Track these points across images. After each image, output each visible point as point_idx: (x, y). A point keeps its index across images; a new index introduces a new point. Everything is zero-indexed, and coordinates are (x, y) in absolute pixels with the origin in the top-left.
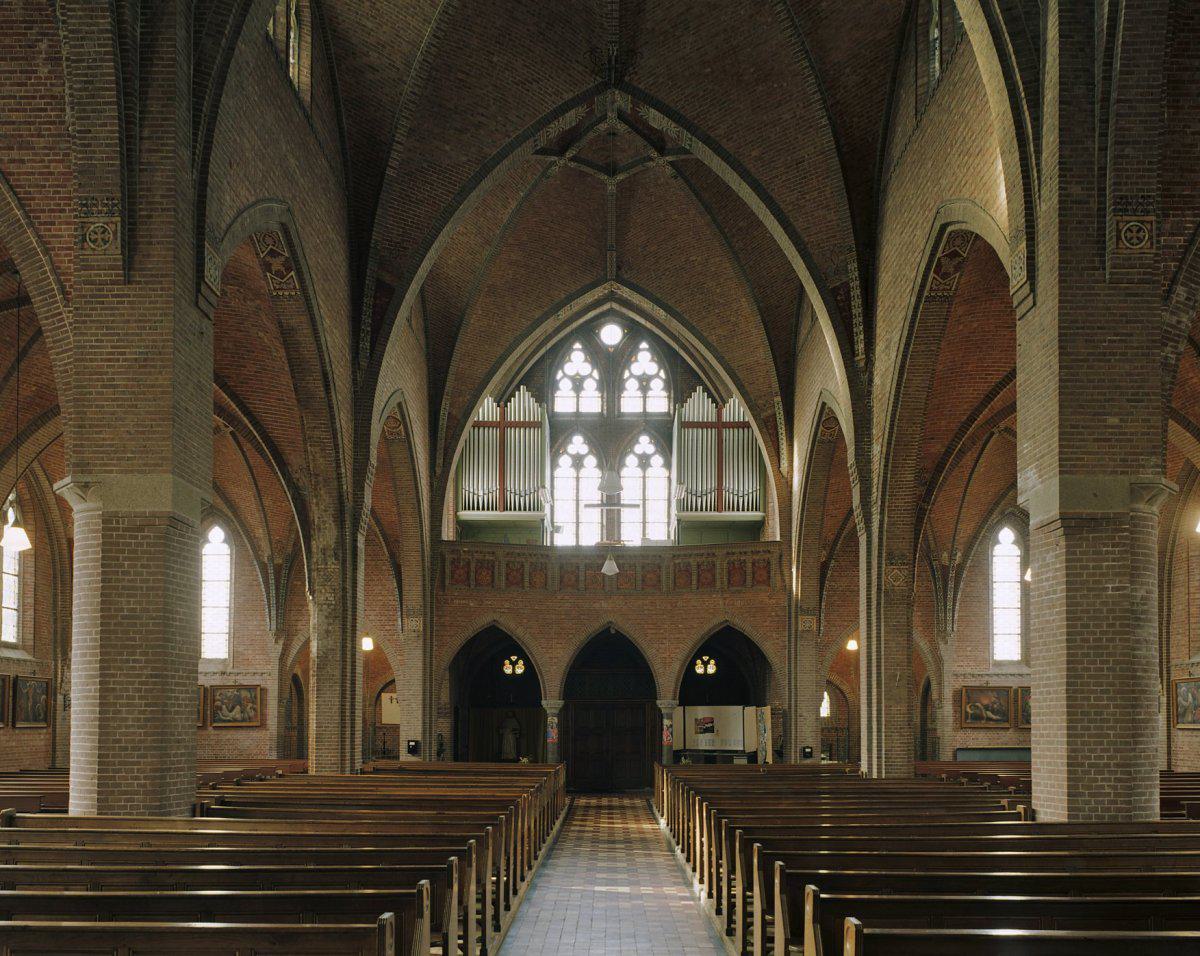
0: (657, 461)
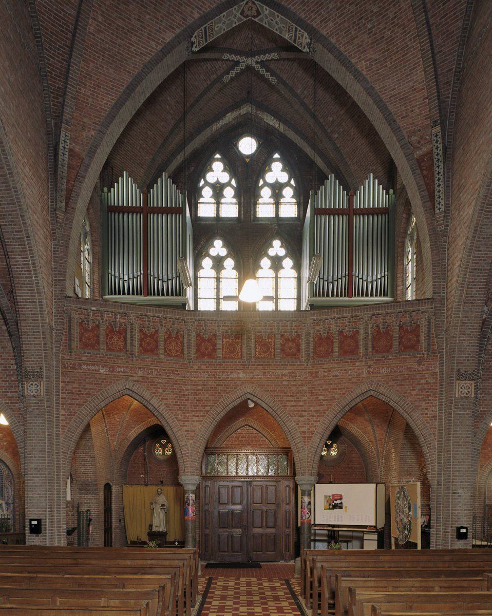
0: (288, 263)
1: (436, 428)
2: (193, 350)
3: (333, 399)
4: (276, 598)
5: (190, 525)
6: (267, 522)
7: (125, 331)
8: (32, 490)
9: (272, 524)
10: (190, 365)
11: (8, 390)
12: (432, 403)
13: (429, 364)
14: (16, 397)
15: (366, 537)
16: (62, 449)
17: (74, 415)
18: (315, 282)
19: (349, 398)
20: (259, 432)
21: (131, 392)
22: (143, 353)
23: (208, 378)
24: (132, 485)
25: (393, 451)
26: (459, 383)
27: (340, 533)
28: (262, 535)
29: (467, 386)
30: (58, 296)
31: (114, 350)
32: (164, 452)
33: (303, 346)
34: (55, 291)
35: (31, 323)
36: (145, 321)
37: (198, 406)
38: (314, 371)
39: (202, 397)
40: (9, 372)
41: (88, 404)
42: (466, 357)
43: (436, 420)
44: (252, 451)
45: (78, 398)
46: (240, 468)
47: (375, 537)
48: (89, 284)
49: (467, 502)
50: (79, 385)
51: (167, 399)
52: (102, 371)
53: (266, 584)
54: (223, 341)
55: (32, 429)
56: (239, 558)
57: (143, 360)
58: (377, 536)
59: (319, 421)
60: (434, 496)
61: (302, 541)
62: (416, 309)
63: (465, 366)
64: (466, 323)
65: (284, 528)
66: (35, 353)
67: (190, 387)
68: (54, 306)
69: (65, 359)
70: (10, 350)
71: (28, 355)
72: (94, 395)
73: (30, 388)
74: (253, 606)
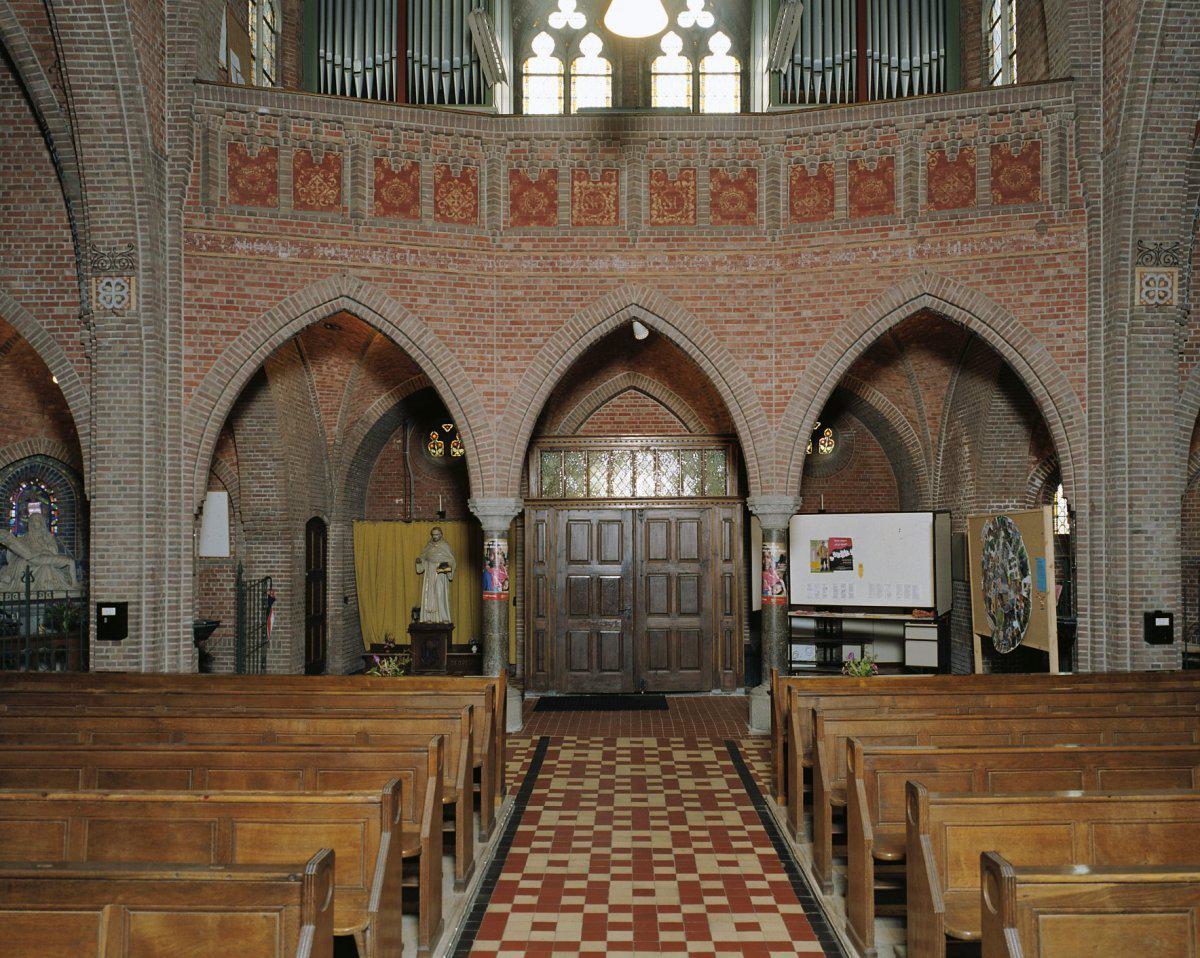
0: (721, 43)
1: (1083, 381)
2: (504, 206)
3: (836, 316)
4: (708, 800)
5: (496, 612)
6: (679, 600)
7: (339, 163)
8: (104, 533)
9: (691, 606)
10: (494, 241)
11: (56, 300)
12: (1071, 322)
13: (1064, 233)
14: (74, 317)
15: (911, 633)
16: (186, 436)
17: (216, 358)
18: (784, 71)
19: (873, 313)
20: (661, 403)
21: (354, 304)
22: (384, 215)
23: (538, 270)
24: (374, 520)
25: (964, 439)
26: (1142, 273)
27: (846, 626)
28: (668, 632)
29: (1162, 279)
30: (177, 81)
31: (312, 208)
32: (447, 449)
33: (763, 197)
34: (170, 68)
35: (106, 138)
36: (386, 140)
37: (514, 335)
38: (789, 252)
39: (523, 314)
40: (58, 259)
41: (249, 331)
42: (1158, 211)
43: (1083, 361)
44: (644, 443)
45: (225, 317)
46: (617, 480)
47: (932, 633)
48: (273, 79)
49: (1168, 552)
50: (228, 289)
51: (441, 320)
52: (283, 256)
53: (680, 755)
54: (573, 188)
55: (108, 388)
56: (616, 684)
57: (382, 231)
58: (936, 630)
59: (804, 368)
60: (1085, 539)
61: (766, 647)
62: (1030, 104)
63: (1155, 232)
64: (1160, 129)
65: (720, 615)
66: (117, 208)
67: (494, 293)
68: (167, 105)
69: (195, 228)
70: (61, 207)
71: (98, 216)
72: (265, 310)
73: (103, 293)
74: (646, 827)
